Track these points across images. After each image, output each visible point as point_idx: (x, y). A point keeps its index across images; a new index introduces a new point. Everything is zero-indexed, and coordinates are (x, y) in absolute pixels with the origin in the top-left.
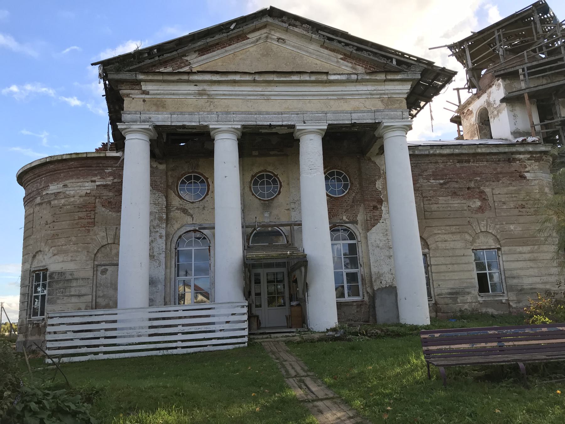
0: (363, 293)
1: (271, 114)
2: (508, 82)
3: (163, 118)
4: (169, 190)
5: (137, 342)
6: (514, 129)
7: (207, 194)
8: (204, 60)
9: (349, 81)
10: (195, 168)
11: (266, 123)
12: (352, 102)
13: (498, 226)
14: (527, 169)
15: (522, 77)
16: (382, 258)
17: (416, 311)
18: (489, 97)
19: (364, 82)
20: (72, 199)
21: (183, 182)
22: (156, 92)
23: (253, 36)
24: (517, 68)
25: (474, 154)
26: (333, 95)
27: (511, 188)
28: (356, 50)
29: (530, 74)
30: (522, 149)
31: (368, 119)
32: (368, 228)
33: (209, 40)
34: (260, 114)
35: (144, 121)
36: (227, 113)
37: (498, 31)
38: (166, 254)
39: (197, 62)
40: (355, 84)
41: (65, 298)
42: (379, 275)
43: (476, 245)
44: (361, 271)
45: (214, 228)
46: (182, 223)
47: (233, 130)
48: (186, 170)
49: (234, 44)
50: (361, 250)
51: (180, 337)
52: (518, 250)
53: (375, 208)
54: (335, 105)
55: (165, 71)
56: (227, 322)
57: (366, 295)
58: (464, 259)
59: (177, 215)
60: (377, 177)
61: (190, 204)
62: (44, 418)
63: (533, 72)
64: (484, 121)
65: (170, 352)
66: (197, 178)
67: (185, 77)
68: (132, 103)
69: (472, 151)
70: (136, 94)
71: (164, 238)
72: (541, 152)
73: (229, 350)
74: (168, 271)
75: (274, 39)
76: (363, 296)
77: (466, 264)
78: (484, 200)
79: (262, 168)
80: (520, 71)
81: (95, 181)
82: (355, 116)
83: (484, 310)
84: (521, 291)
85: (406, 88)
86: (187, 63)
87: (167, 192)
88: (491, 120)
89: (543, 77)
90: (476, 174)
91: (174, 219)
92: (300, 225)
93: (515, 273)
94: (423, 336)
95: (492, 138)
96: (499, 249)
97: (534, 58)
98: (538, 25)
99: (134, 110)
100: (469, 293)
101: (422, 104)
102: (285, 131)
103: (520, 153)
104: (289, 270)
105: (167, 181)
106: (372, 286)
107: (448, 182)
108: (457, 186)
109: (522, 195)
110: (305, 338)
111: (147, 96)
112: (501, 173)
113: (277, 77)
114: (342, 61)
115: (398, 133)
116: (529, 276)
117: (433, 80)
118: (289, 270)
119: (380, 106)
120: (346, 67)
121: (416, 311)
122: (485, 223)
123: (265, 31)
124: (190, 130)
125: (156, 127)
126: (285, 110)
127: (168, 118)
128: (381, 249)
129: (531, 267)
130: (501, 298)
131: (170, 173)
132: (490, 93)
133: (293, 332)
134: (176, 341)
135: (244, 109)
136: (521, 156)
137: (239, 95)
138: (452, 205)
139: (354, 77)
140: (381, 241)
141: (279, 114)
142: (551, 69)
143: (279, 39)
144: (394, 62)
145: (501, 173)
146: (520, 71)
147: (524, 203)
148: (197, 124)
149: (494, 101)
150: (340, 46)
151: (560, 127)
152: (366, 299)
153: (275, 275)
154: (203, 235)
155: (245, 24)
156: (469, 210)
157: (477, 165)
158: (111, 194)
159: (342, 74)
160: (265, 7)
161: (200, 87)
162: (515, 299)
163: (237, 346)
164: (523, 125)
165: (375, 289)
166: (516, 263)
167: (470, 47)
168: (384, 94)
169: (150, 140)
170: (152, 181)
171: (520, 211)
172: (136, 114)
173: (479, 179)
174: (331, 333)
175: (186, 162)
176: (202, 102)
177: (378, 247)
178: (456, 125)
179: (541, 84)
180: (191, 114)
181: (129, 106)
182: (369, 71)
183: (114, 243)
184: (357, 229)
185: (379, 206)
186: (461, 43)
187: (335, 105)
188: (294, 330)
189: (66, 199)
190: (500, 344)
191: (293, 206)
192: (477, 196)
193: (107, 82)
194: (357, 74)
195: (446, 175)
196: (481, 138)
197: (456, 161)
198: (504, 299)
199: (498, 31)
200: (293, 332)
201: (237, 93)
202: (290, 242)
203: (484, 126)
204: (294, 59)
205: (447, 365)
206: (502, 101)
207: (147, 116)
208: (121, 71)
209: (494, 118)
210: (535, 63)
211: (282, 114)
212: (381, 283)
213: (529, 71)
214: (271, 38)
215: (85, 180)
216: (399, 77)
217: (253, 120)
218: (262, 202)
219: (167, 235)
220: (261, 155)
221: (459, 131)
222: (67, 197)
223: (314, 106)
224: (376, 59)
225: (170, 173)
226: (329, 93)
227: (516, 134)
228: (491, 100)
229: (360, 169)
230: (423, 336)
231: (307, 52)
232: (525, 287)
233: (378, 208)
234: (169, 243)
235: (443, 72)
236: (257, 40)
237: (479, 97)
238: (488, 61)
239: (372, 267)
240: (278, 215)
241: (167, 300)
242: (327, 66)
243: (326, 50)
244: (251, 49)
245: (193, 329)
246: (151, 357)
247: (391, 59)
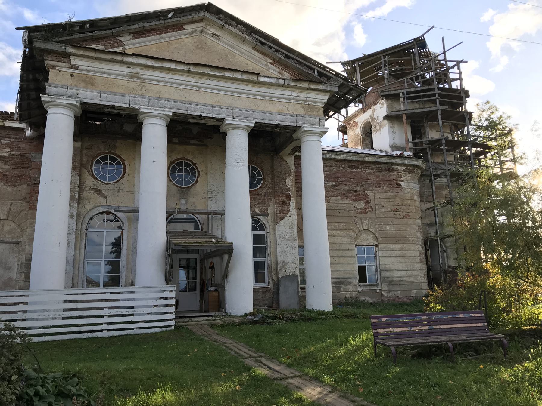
0: (269, 280)
1: (202, 106)
2: (390, 102)
3: (91, 96)
4: (83, 169)
5: (52, 325)
6: (392, 143)
7: (123, 176)
8: (138, 43)
9: (276, 85)
10: (112, 149)
11: (196, 114)
12: (277, 105)
13: (377, 226)
14: (402, 179)
15: (402, 100)
16: (288, 249)
17: (321, 299)
18: (373, 112)
19: (289, 87)
21: (98, 162)
22: (86, 68)
23: (189, 28)
24: (399, 91)
25: (362, 161)
26: (261, 95)
27: (389, 194)
28: (284, 57)
29: (409, 98)
30: (400, 161)
31: (290, 122)
32: (276, 222)
33: (146, 24)
34: (192, 104)
35: (71, 97)
36: (159, 99)
37: (385, 57)
38: (76, 235)
39: (131, 44)
40: (281, 88)
42: (284, 264)
43: (359, 242)
44: (267, 260)
45: (138, 212)
46: (94, 203)
47: (164, 116)
48: (103, 150)
49: (170, 32)
50: (269, 241)
51: (106, 320)
52: (391, 247)
53: (284, 203)
54: (263, 106)
55: (97, 48)
56: (155, 306)
57: (271, 282)
58: (349, 253)
59: (90, 195)
60: (287, 175)
61: (105, 185)
62: (52, 402)
63: (412, 97)
64: (367, 133)
65: (95, 335)
66: (113, 159)
67: (119, 58)
68: (58, 77)
69: (361, 159)
70: (63, 66)
71: (75, 218)
72: (414, 166)
73: (156, 333)
74: (78, 252)
76: (269, 283)
77: (349, 257)
78: (367, 202)
79: (181, 156)
80: (401, 94)
82: (279, 118)
83: (362, 298)
84: (391, 283)
85: (325, 98)
87: (80, 170)
88: (374, 133)
89: (417, 102)
90: (363, 179)
91: (86, 199)
92: (222, 214)
93: (388, 267)
94: (373, 321)
95: (372, 148)
96: (376, 246)
97: (411, 86)
98: (417, 58)
99: (60, 83)
100: (351, 283)
101: (331, 113)
102: (214, 123)
103: (398, 164)
104: (202, 257)
105: (81, 160)
106: (277, 274)
107: (339, 185)
108: (346, 188)
109: (398, 201)
110: (227, 322)
112: (382, 180)
113: (212, 71)
114: (271, 65)
115: (315, 138)
116: (399, 270)
117: (345, 94)
118: (202, 257)
119: (301, 111)
120: (274, 71)
121: (321, 299)
122: (367, 222)
123: (200, 24)
124: (118, 111)
125: (83, 104)
126: (216, 104)
127: (97, 96)
128: (287, 240)
129: (401, 263)
131: (85, 152)
132: (375, 109)
133: (212, 316)
134: (102, 324)
135: (176, 97)
136: (399, 168)
137: (171, 83)
138: (341, 205)
139: (281, 82)
140: (287, 233)
141: (210, 106)
142: (424, 96)
143: (214, 35)
144: (316, 73)
145: (382, 180)
146: (401, 94)
147: (398, 207)
148: (128, 106)
149: (378, 117)
151: (428, 146)
152: (271, 285)
153: (197, 262)
154: (124, 217)
155: (183, 14)
156: (355, 210)
157: (364, 171)
158: (7, 167)
159: (271, 77)
160: (204, 2)
161: (133, 70)
162: (387, 289)
163: (164, 329)
164: (400, 140)
165: (280, 277)
166: (390, 258)
167: (361, 67)
168: (306, 101)
169: (75, 116)
171: (395, 214)
172: (62, 87)
173: (364, 183)
174: (251, 317)
175: (103, 142)
176: (133, 84)
177: (285, 238)
178: (341, 134)
179: (416, 107)
180: (121, 95)
181: (55, 78)
182: (293, 78)
183: (7, 219)
184: (267, 221)
185: (287, 202)
186: (353, 62)
187: (263, 106)
188: (213, 314)
190: (431, 327)
191: (210, 195)
192: (361, 198)
193: (28, 50)
194: (284, 79)
195: (338, 178)
196: (364, 148)
197: (347, 166)
199: (385, 57)
200: (212, 316)
201: (170, 80)
202: (205, 230)
203: (366, 138)
204: (227, 56)
205: (397, 345)
206: (385, 117)
207: (75, 91)
208: (49, 40)
209: (376, 132)
210: (413, 90)
211: (213, 107)
212: (285, 271)
213: (408, 96)
214: (206, 33)
216: (320, 87)
217: (184, 109)
218: (180, 189)
219: (79, 216)
220: (180, 143)
221: (344, 139)
223: (243, 103)
224: (301, 68)
225: (85, 152)
226: (245, 91)
227: (394, 147)
228: (375, 116)
229: (272, 167)
230: (373, 321)
231: (240, 51)
232: (395, 279)
233: (286, 203)
234: (80, 224)
235: (356, 89)
236: (193, 33)
237: (364, 112)
238: (374, 81)
239: (278, 257)
240: (196, 201)
241: (75, 281)
242: (256, 67)
243: (257, 53)
244: (186, 40)
245: (120, 312)
246: (75, 340)
247: (314, 70)
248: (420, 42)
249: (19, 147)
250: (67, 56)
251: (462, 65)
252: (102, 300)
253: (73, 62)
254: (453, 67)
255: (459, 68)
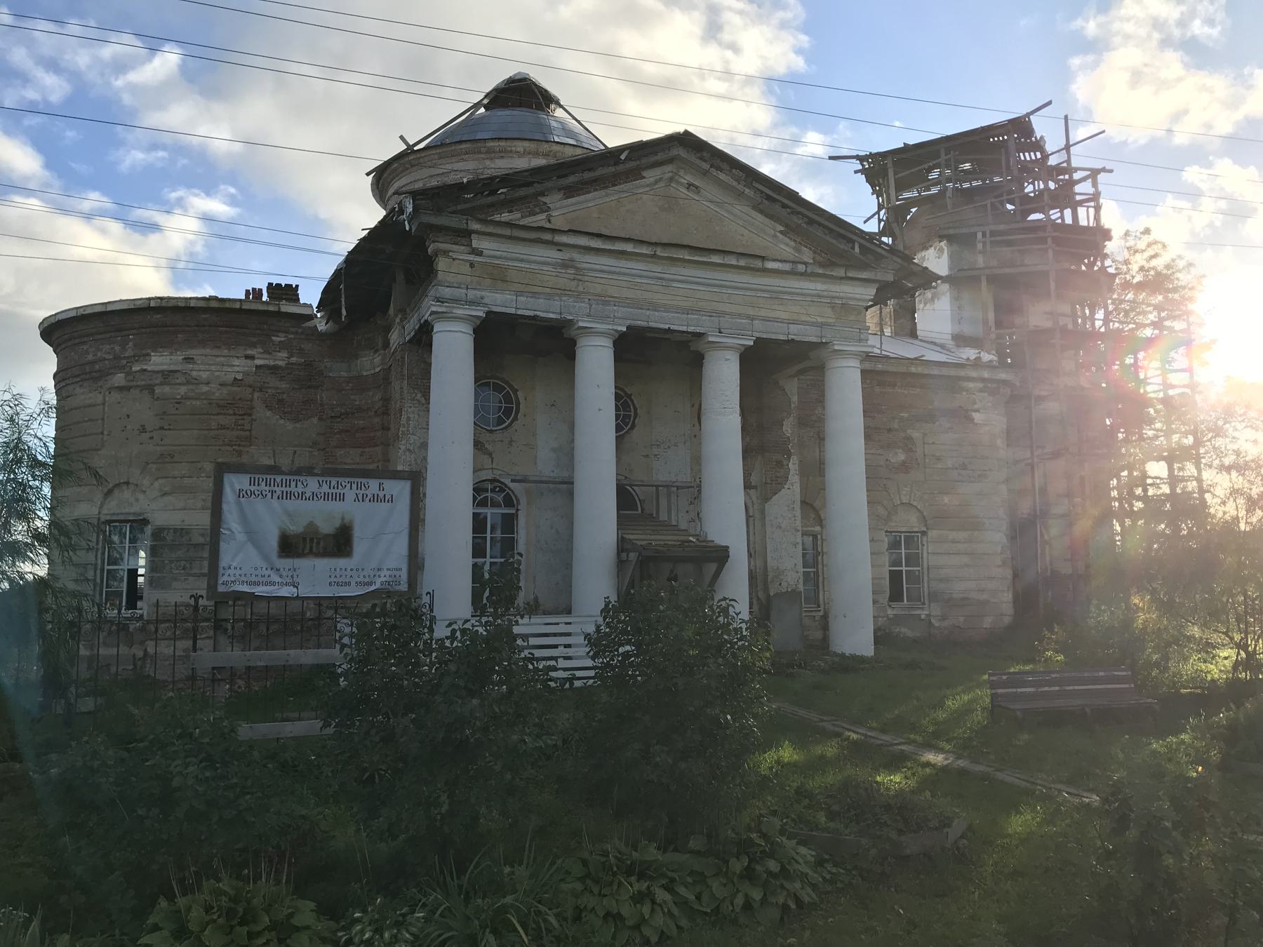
3: (503, 301)
7: (515, 419)
9: (793, 273)
11: (662, 326)
15: (980, 246)
20: (205, 389)
23: (651, 175)
28: (807, 223)
31: (811, 336)
41: (191, 578)
69: (902, 369)
70: (460, 252)
75: (682, 184)
80: (979, 235)
81: (252, 358)
86: (544, 207)
96: (924, 533)
106: (766, 589)
111: (478, 259)
120: (786, 247)
121: (856, 635)
130: (918, 612)
136: (971, 385)
137: (624, 274)
139: (801, 268)
144: (857, 249)
146: (979, 235)
150: (784, 212)
158: (284, 385)
170: (476, 407)
189: (191, 387)
191: (655, 451)
198: (923, 614)
215: (233, 353)
216: (864, 275)
222: (197, 382)
232: (955, 596)
236: (656, 182)
244: (645, 197)
247: (853, 242)
248: (1020, 127)
249: (301, 349)
250: (467, 234)
251: (1101, 177)
252: (555, 635)
253: (475, 244)
254: (1083, 179)
255: (1095, 184)
